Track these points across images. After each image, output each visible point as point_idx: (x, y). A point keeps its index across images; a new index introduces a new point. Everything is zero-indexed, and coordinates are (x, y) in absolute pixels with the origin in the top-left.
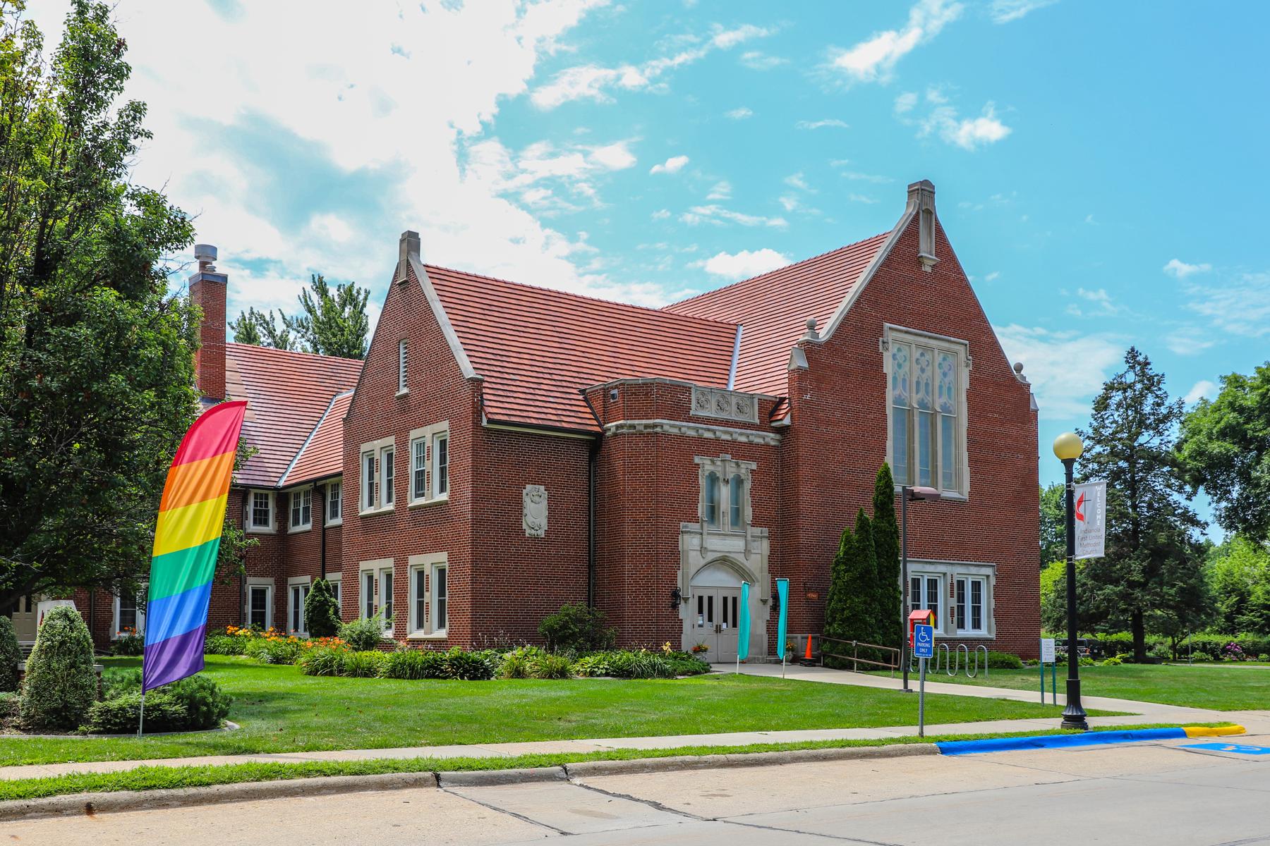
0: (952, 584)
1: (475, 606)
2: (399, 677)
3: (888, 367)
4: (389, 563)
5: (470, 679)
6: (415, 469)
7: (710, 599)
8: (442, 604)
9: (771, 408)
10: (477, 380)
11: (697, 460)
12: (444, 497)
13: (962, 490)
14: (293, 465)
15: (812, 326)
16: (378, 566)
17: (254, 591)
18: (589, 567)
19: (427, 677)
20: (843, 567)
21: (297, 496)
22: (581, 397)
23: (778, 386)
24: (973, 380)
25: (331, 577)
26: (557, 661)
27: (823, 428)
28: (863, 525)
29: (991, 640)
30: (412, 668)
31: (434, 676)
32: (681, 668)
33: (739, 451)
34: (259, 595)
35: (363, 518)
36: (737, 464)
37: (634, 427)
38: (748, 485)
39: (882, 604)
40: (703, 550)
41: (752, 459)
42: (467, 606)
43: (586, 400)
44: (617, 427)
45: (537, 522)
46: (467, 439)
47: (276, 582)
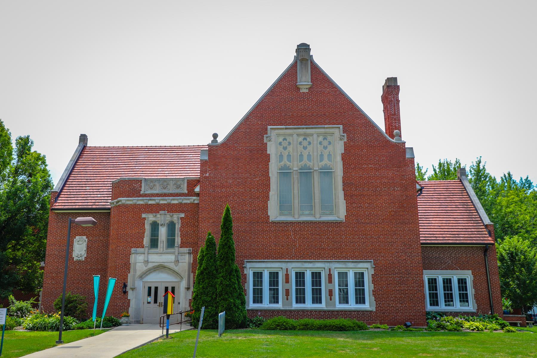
7: (156, 288)
9: (192, 183)
11: (144, 216)
13: (341, 213)
33: (171, 208)
38: (178, 226)
40: (147, 262)
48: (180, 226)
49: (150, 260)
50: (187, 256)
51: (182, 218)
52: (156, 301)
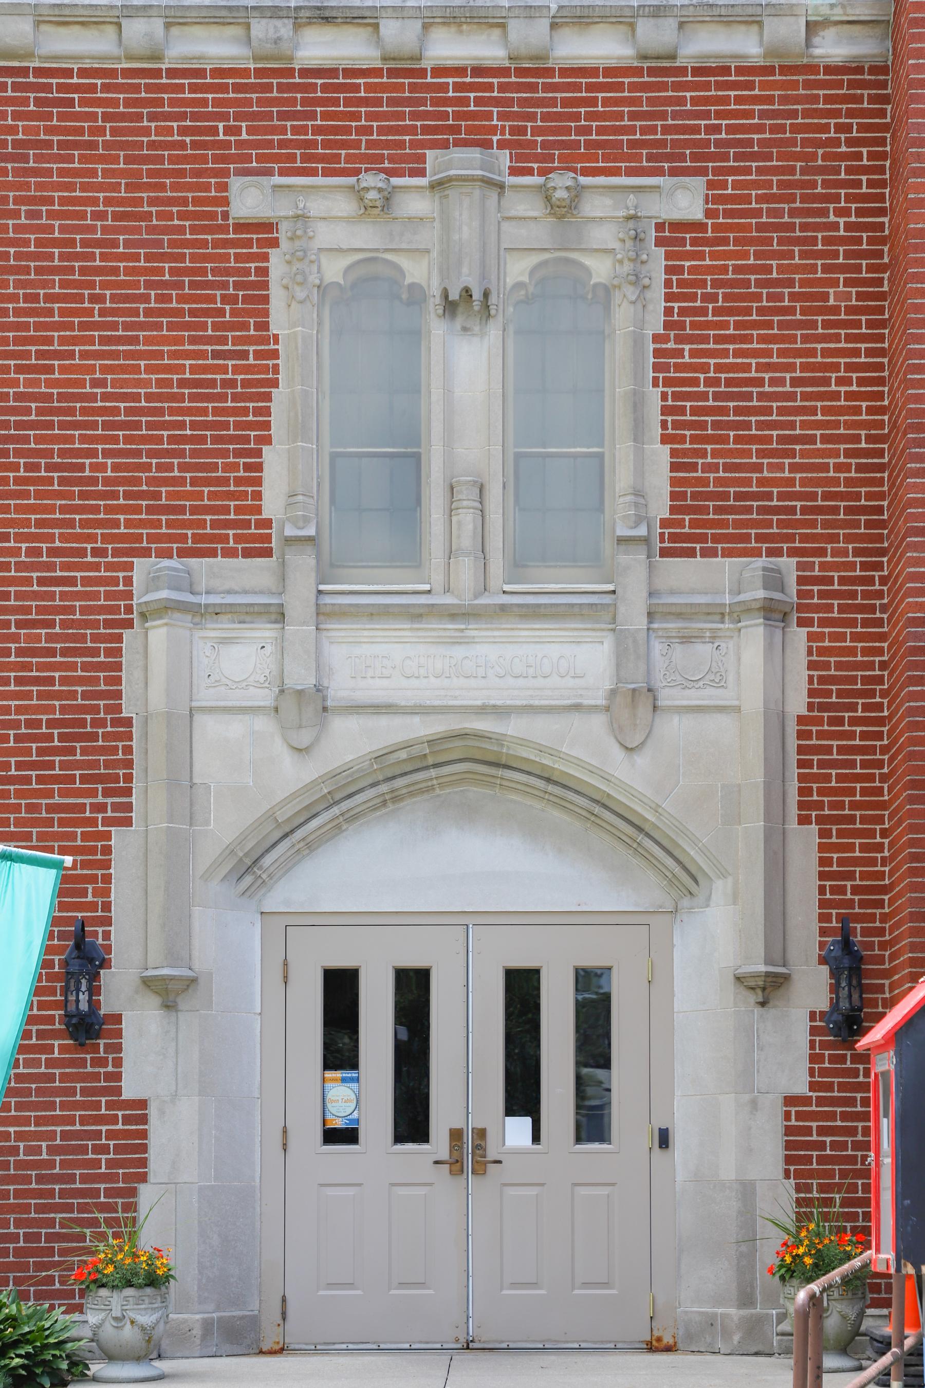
7: (413, 988)
11: (248, 199)
40: (306, 706)
48: (656, 323)
49: (341, 687)
50: (753, 638)
51: (673, 234)
52: (412, 1122)
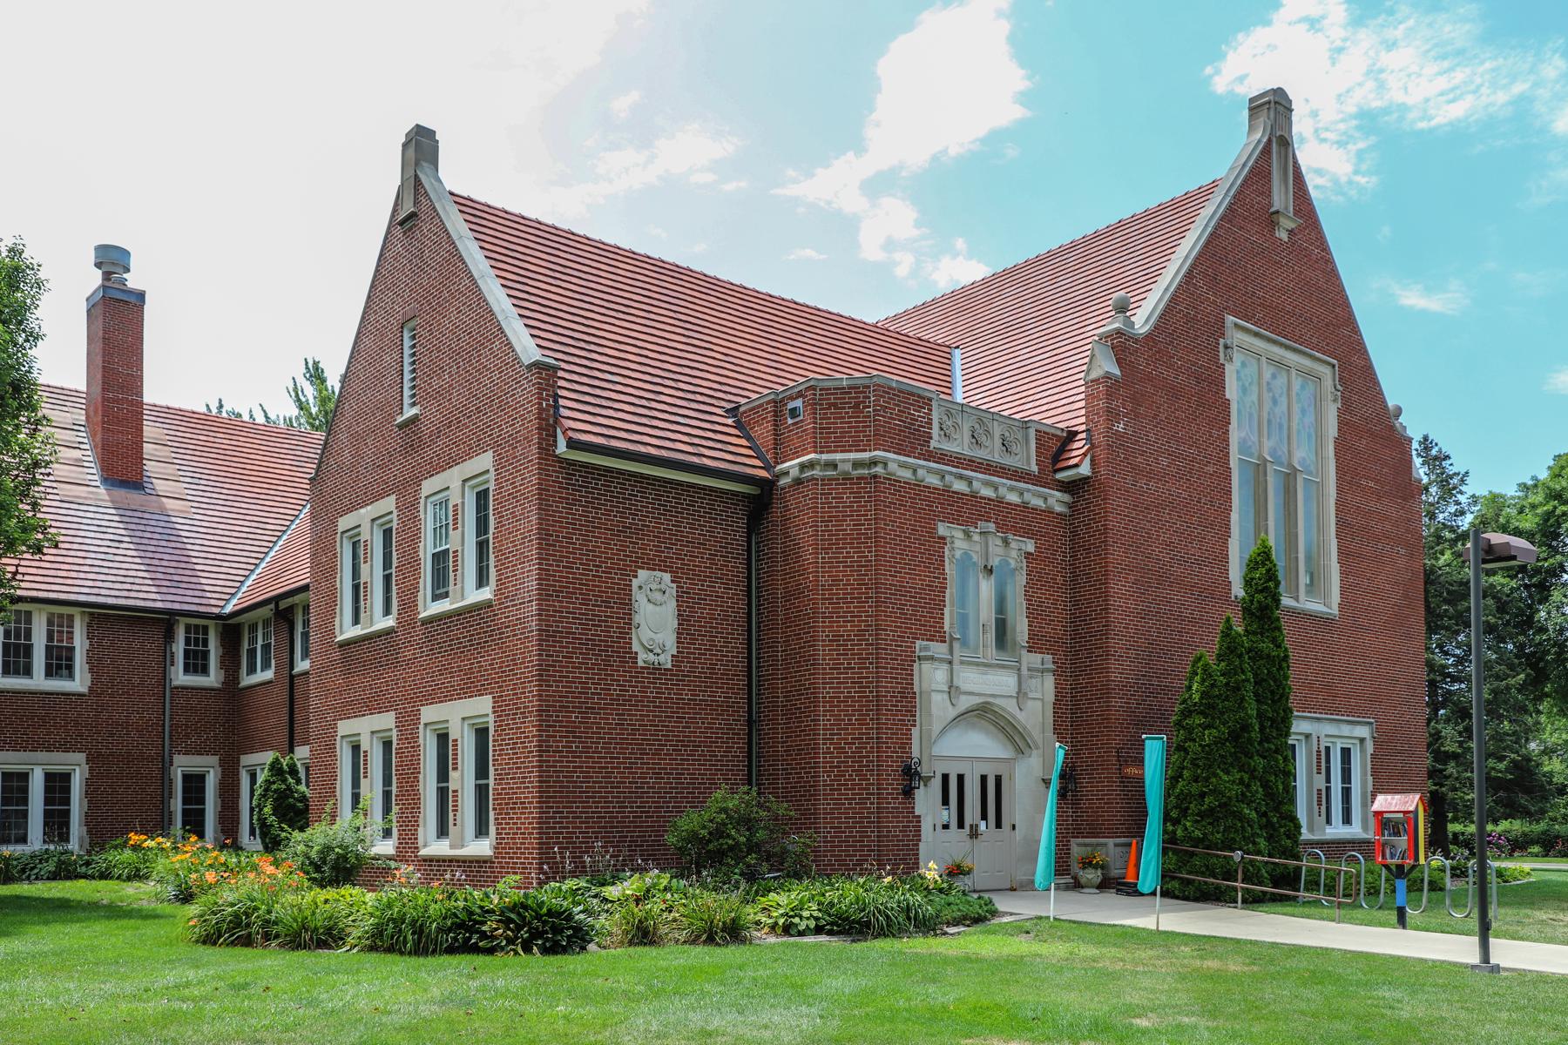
0: (1319, 751)
1: (544, 797)
2: (390, 950)
3: (1232, 391)
4: (387, 721)
5: (546, 951)
6: (430, 551)
7: (961, 778)
8: (482, 792)
9: (1056, 446)
10: (547, 367)
11: (942, 529)
12: (486, 594)
14: (249, 582)
15: (1122, 308)
16: (368, 728)
17: (186, 777)
18: (750, 722)
19: (451, 950)
20: (1199, 720)
21: (253, 628)
22: (730, 421)
23: (1065, 408)
24: (1342, 424)
25: (302, 752)
26: (717, 903)
27: (1142, 483)
28: (1230, 648)
29: (1368, 842)
30: (419, 930)
31: (468, 949)
32: (948, 914)
33: (1012, 520)
34: (194, 784)
35: (345, 645)
36: (1006, 542)
37: (833, 465)
39: (1265, 785)
40: (952, 690)
41: (1028, 533)
42: (530, 795)
43: (738, 425)
44: (803, 467)
45: (659, 638)
46: (530, 478)
47: (222, 763)
